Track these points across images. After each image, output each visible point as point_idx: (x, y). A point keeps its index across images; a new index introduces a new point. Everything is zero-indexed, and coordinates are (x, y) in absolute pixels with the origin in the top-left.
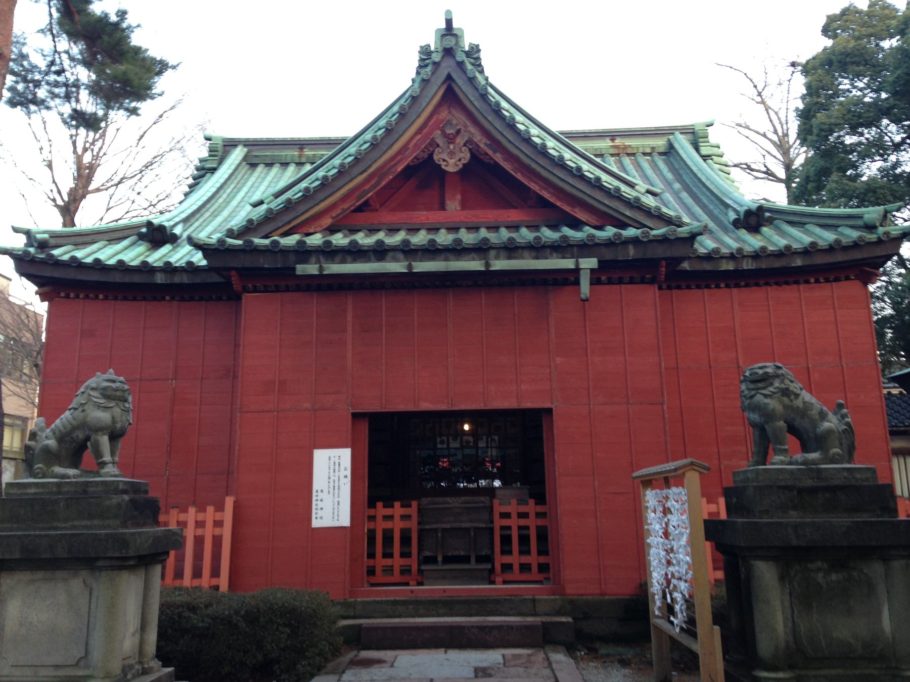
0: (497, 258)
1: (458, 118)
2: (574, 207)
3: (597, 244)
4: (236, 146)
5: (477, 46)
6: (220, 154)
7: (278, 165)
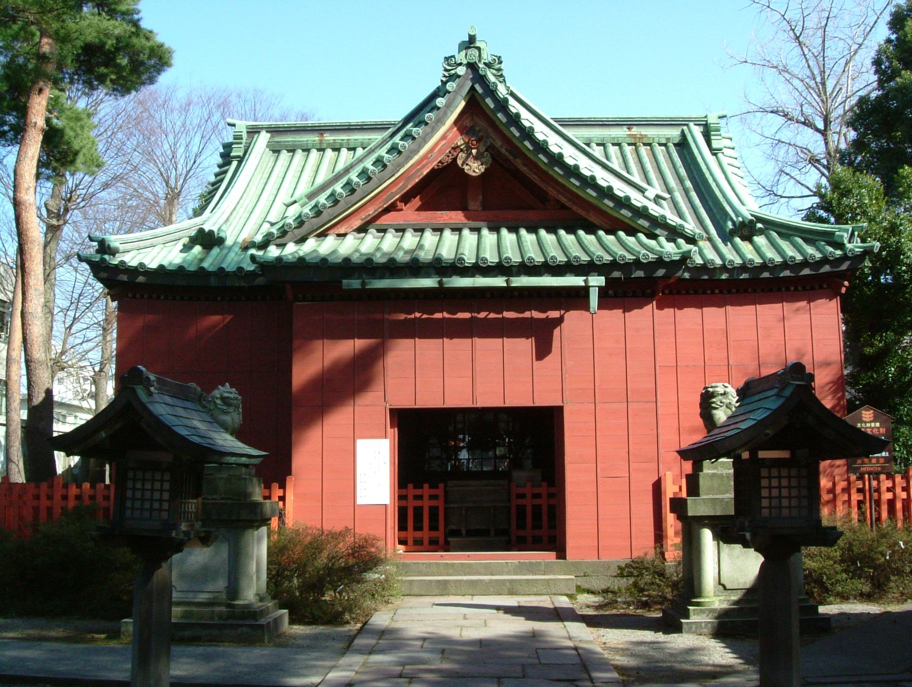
4: (259, 132)
5: (499, 58)
6: (244, 141)
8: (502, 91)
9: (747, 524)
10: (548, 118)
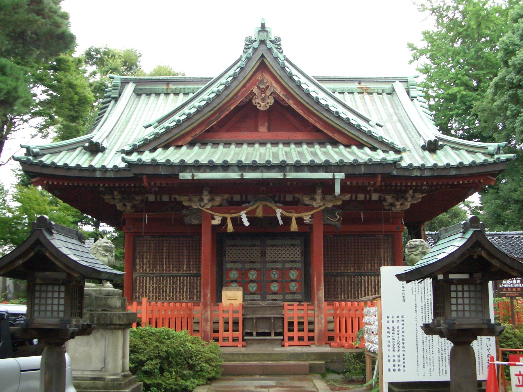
0: (290, 171)
1: (268, 78)
2: (334, 133)
3: (344, 165)
4: (129, 83)
5: (279, 38)
6: (119, 88)
7: (154, 95)
8: (281, 56)
9: (442, 322)
10: (310, 76)
